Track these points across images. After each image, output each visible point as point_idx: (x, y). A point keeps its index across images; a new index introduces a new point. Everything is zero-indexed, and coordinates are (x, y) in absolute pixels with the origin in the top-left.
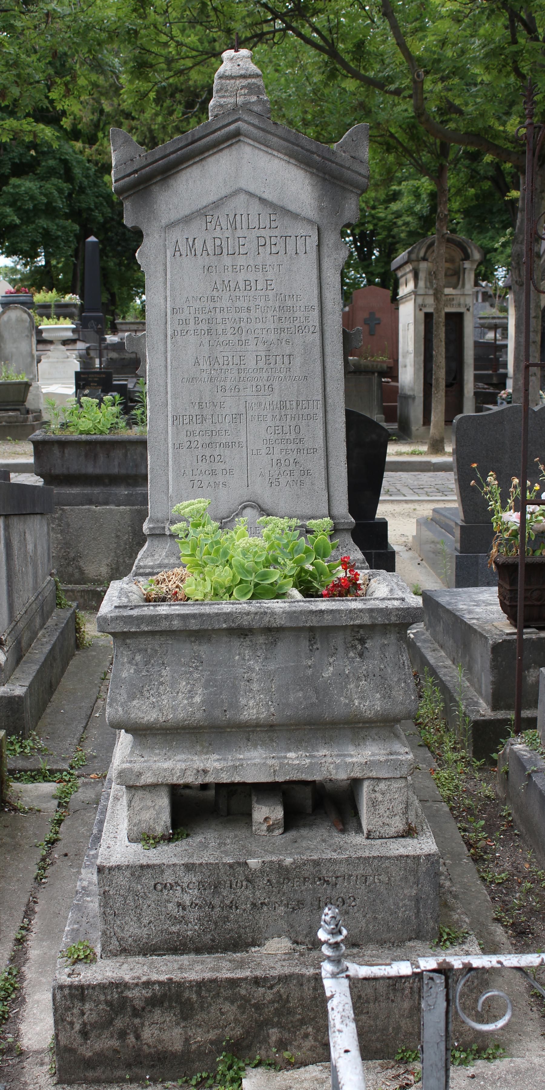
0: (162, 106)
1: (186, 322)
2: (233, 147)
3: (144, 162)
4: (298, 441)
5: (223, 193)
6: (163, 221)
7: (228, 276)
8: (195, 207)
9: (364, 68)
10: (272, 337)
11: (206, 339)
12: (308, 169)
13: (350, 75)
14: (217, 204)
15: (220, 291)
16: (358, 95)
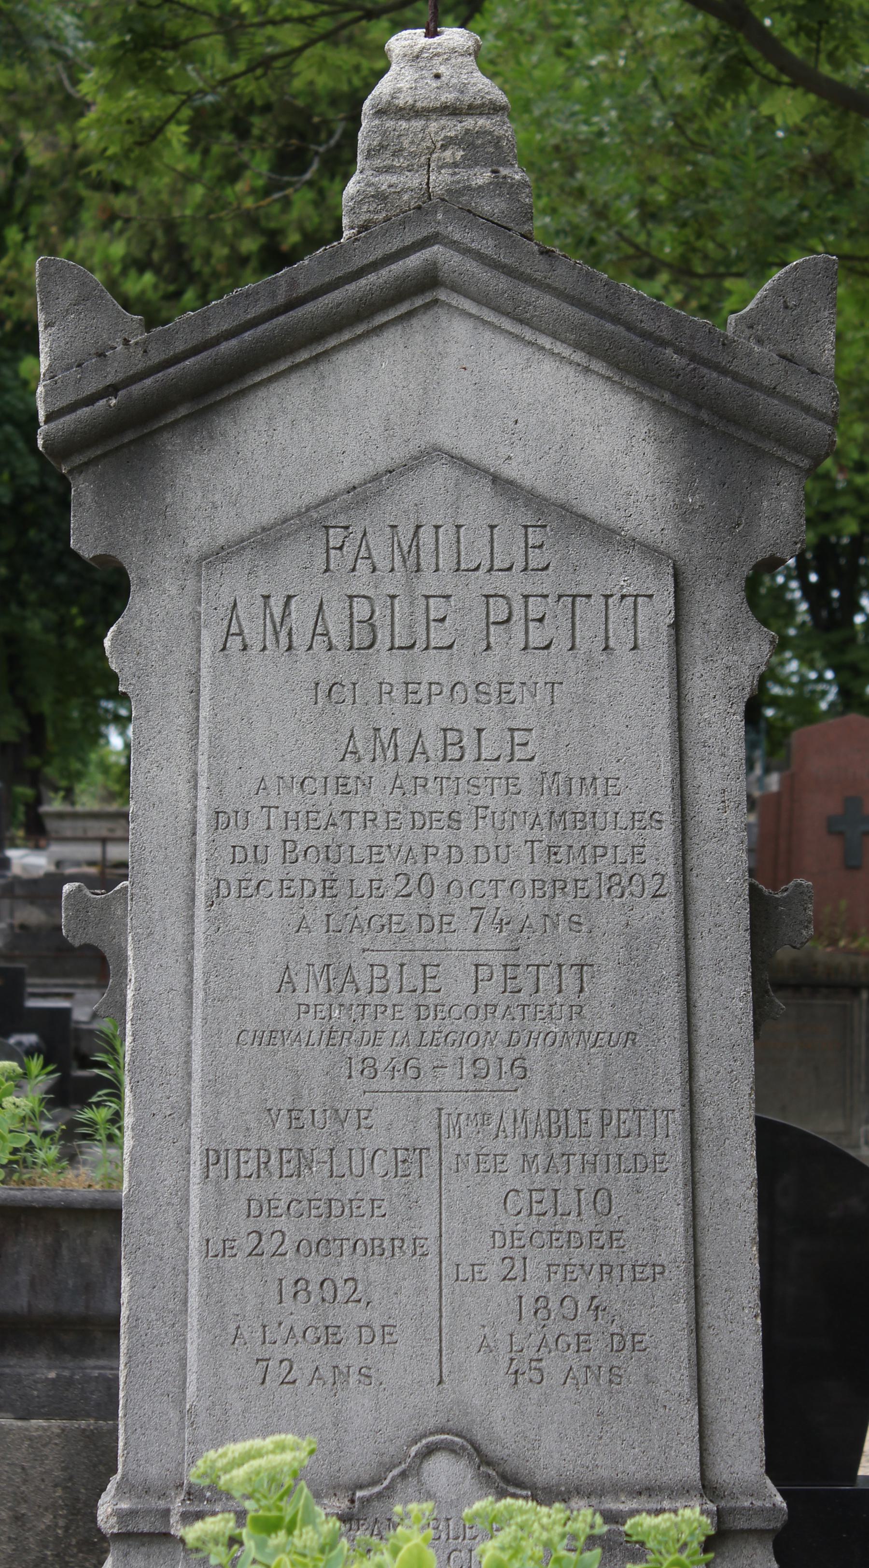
0: (206, 152)
1: (257, 855)
2: (414, 321)
3: (139, 363)
4: (604, 1238)
5: (381, 460)
6: (192, 543)
7: (392, 714)
8: (292, 503)
9: (832, 57)
10: (527, 907)
11: (317, 910)
12: (646, 391)
13: (785, 79)
14: (362, 494)
15: (366, 761)
16: (813, 134)
